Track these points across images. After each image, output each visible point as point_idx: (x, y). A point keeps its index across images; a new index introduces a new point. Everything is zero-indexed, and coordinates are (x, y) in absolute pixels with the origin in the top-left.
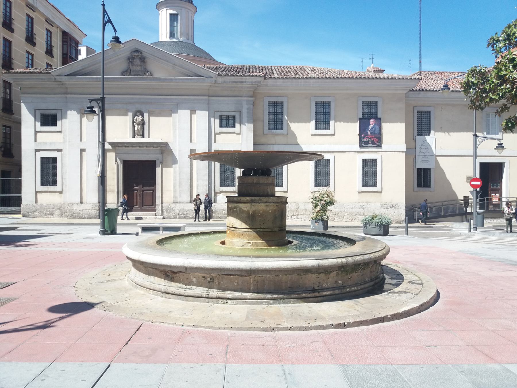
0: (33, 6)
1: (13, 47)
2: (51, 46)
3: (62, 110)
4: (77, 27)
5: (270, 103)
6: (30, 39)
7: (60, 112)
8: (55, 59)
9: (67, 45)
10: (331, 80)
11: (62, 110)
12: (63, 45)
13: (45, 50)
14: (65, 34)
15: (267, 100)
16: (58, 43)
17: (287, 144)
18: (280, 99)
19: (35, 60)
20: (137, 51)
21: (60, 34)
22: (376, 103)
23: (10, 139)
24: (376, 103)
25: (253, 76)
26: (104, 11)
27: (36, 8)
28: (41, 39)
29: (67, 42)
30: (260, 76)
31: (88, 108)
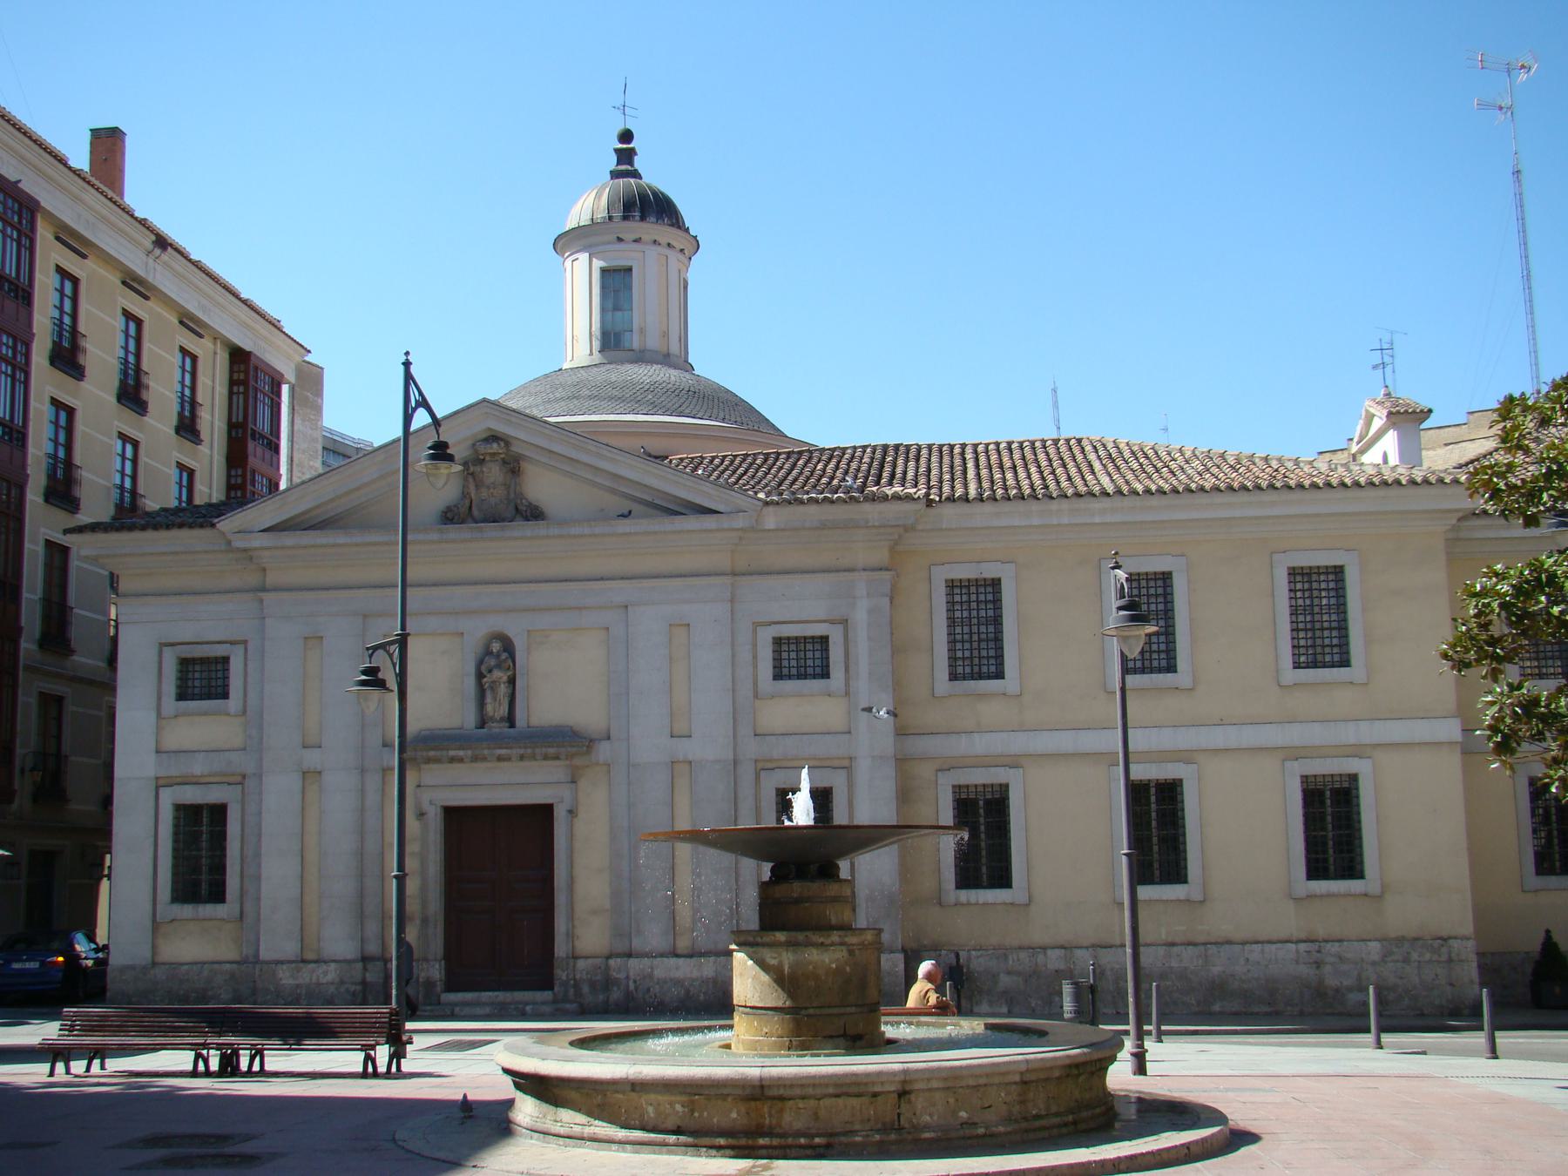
0: (142, 281)
1: (80, 427)
2: (194, 404)
3: (245, 642)
4: (275, 325)
5: (951, 585)
6: (132, 394)
7: (240, 649)
8: (204, 449)
9: (246, 394)
10: (1164, 500)
11: (245, 642)
12: (231, 393)
13: (174, 421)
14: (239, 357)
15: (942, 575)
16: (218, 388)
17: (1022, 729)
18: (989, 572)
19: (143, 459)
20: (494, 438)
21: (223, 358)
22: (1338, 571)
23: (59, 737)
24: (1338, 571)
25: (885, 498)
26: (409, 378)
27: (153, 288)
28: (163, 391)
29: (245, 383)
30: (909, 498)
31: (364, 673)
